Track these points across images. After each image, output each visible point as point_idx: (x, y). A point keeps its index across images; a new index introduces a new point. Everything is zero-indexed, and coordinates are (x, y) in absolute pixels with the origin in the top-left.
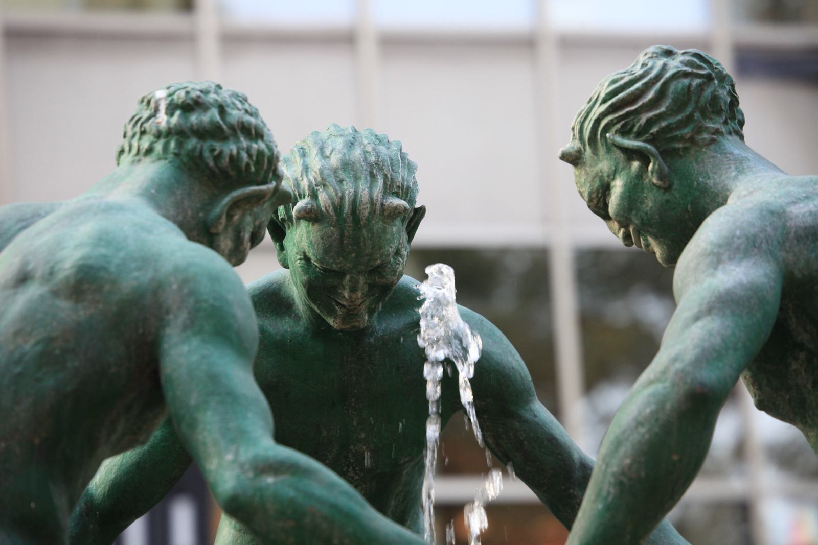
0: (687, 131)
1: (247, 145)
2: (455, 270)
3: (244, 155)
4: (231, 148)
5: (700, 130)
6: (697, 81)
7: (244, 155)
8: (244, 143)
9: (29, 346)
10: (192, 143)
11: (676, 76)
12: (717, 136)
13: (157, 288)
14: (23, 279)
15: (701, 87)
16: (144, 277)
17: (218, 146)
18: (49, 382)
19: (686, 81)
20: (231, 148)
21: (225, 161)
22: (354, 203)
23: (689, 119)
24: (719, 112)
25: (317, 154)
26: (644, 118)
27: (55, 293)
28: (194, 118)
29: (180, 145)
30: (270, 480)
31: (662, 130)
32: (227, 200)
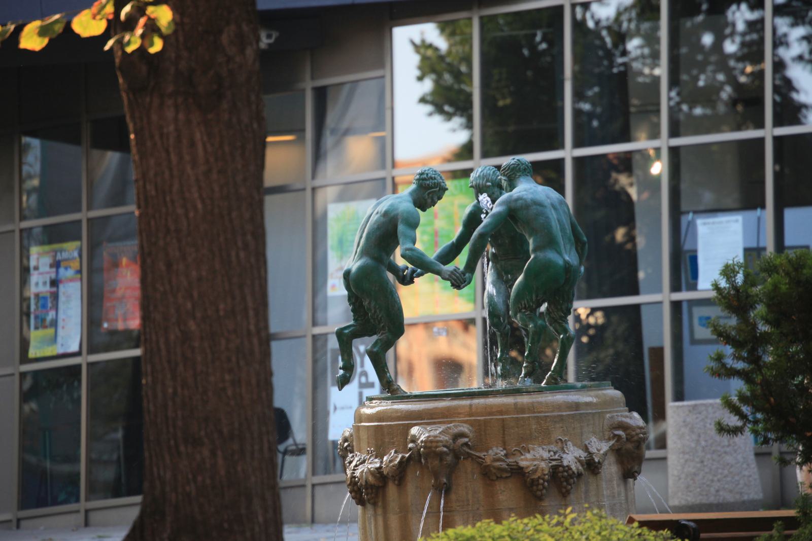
0: (513, 176)
1: (530, 239)
2: (637, 412)
3: (431, 184)
4: (428, 182)
5: (516, 175)
6: (516, 165)
7: (431, 184)
8: (431, 181)
9: (376, 226)
10: (526, 167)
11: (513, 164)
12: (127, 266)
13: (397, 215)
14: (377, 213)
15: (517, 166)
16: (395, 212)
17: (425, 182)
18: (378, 233)
19: (513, 166)
20: (428, 182)
21: (427, 185)
22: (479, 185)
23: (514, 173)
24: (520, 171)
25: (686, 500)
26: (506, 173)
27: (381, 216)
28: (422, 177)
29: (419, 182)
30: (407, 252)
31: (509, 176)
32: (427, 193)
